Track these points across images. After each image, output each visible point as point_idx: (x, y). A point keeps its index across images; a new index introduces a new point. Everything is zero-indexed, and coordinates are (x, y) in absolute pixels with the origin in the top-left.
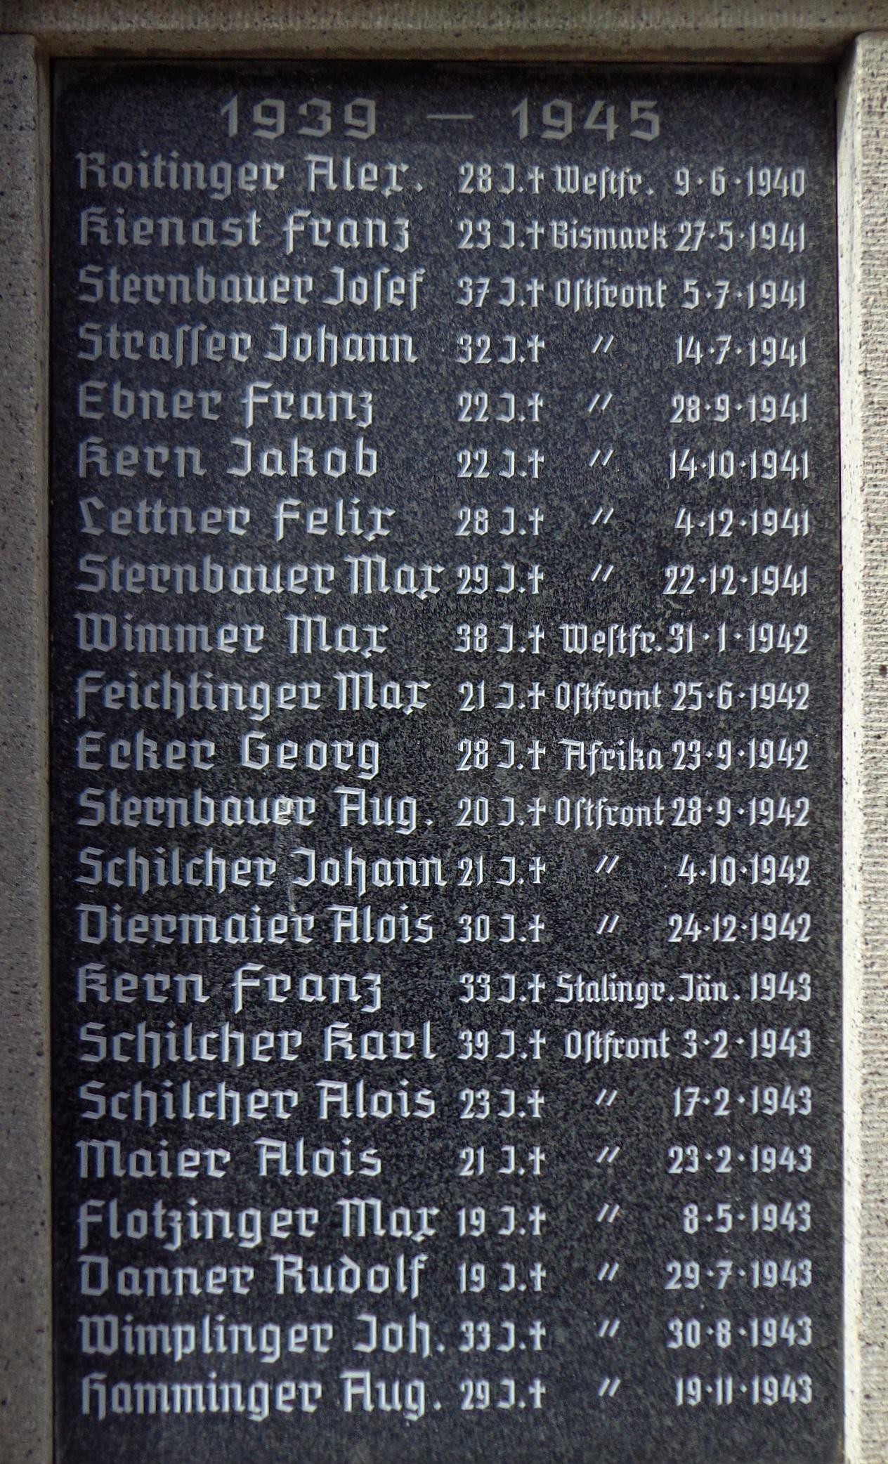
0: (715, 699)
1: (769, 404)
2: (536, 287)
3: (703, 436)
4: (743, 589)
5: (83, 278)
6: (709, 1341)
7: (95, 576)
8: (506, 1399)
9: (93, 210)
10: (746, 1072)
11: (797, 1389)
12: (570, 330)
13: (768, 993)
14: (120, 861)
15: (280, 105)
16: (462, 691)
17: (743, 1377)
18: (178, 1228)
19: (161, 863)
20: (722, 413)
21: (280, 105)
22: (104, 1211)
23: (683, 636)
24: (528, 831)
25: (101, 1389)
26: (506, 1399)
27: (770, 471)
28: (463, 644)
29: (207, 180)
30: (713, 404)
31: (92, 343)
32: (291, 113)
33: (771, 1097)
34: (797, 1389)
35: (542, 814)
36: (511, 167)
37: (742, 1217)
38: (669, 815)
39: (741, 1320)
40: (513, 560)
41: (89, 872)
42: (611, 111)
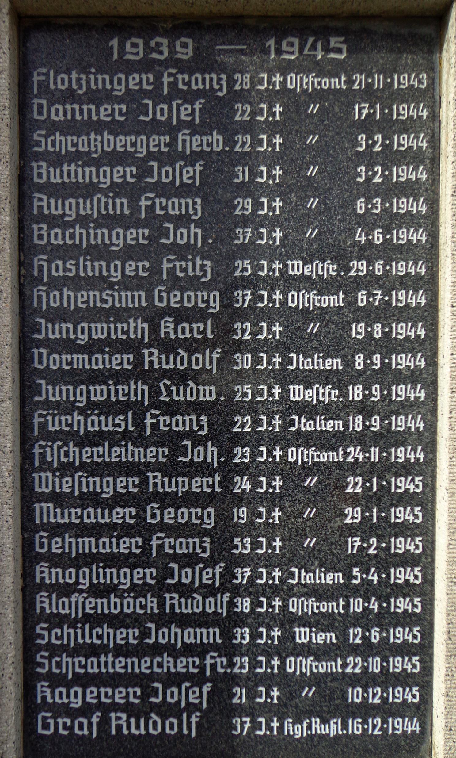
0: (373, 239)
1: (403, 109)
2: (277, 603)
3: (368, 222)
4: (385, 700)
5: (38, 631)
6: (369, 335)
7: (44, 664)
8: (262, 239)
9: (43, 564)
10: (388, 376)
11: (411, 726)
12: (294, 473)
13: (400, 488)
14: (58, 659)
15: (140, 42)
16: (236, 265)
17: (383, 628)
18: (84, 83)
19: (79, 631)
20: (376, 364)
21: (140, 42)
22: (47, 75)
23: (357, 423)
24: (272, 616)
25: (44, 295)
26: (262, 239)
27: (398, 698)
28: (238, 238)
29: (101, 487)
30: (370, 391)
31: (44, 664)
32: (146, 44)
33: (400, 543)
34: (411, 726)
35: (280, 144)
36: (265, 356)
37: (388, 268)
38: (347, 606)
39: (387, 230)
40: (264, 595)
41: (42, 665)
42: (319, 45)
